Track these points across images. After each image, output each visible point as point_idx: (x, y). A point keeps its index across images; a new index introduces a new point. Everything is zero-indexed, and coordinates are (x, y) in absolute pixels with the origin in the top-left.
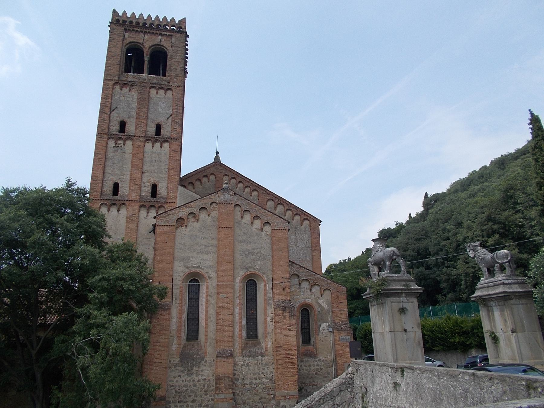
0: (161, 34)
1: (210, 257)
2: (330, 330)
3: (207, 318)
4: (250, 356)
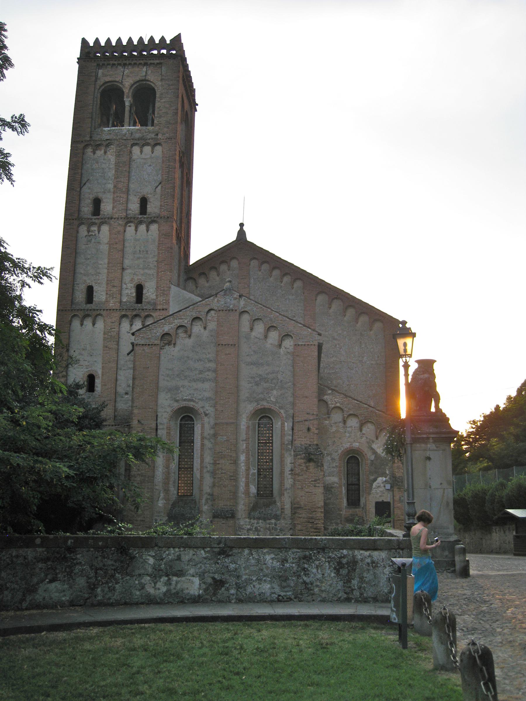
0: (145, 64)
1: (207, 385)
2: (388, 486)
3: (202, 468)
4: (259, 518)
